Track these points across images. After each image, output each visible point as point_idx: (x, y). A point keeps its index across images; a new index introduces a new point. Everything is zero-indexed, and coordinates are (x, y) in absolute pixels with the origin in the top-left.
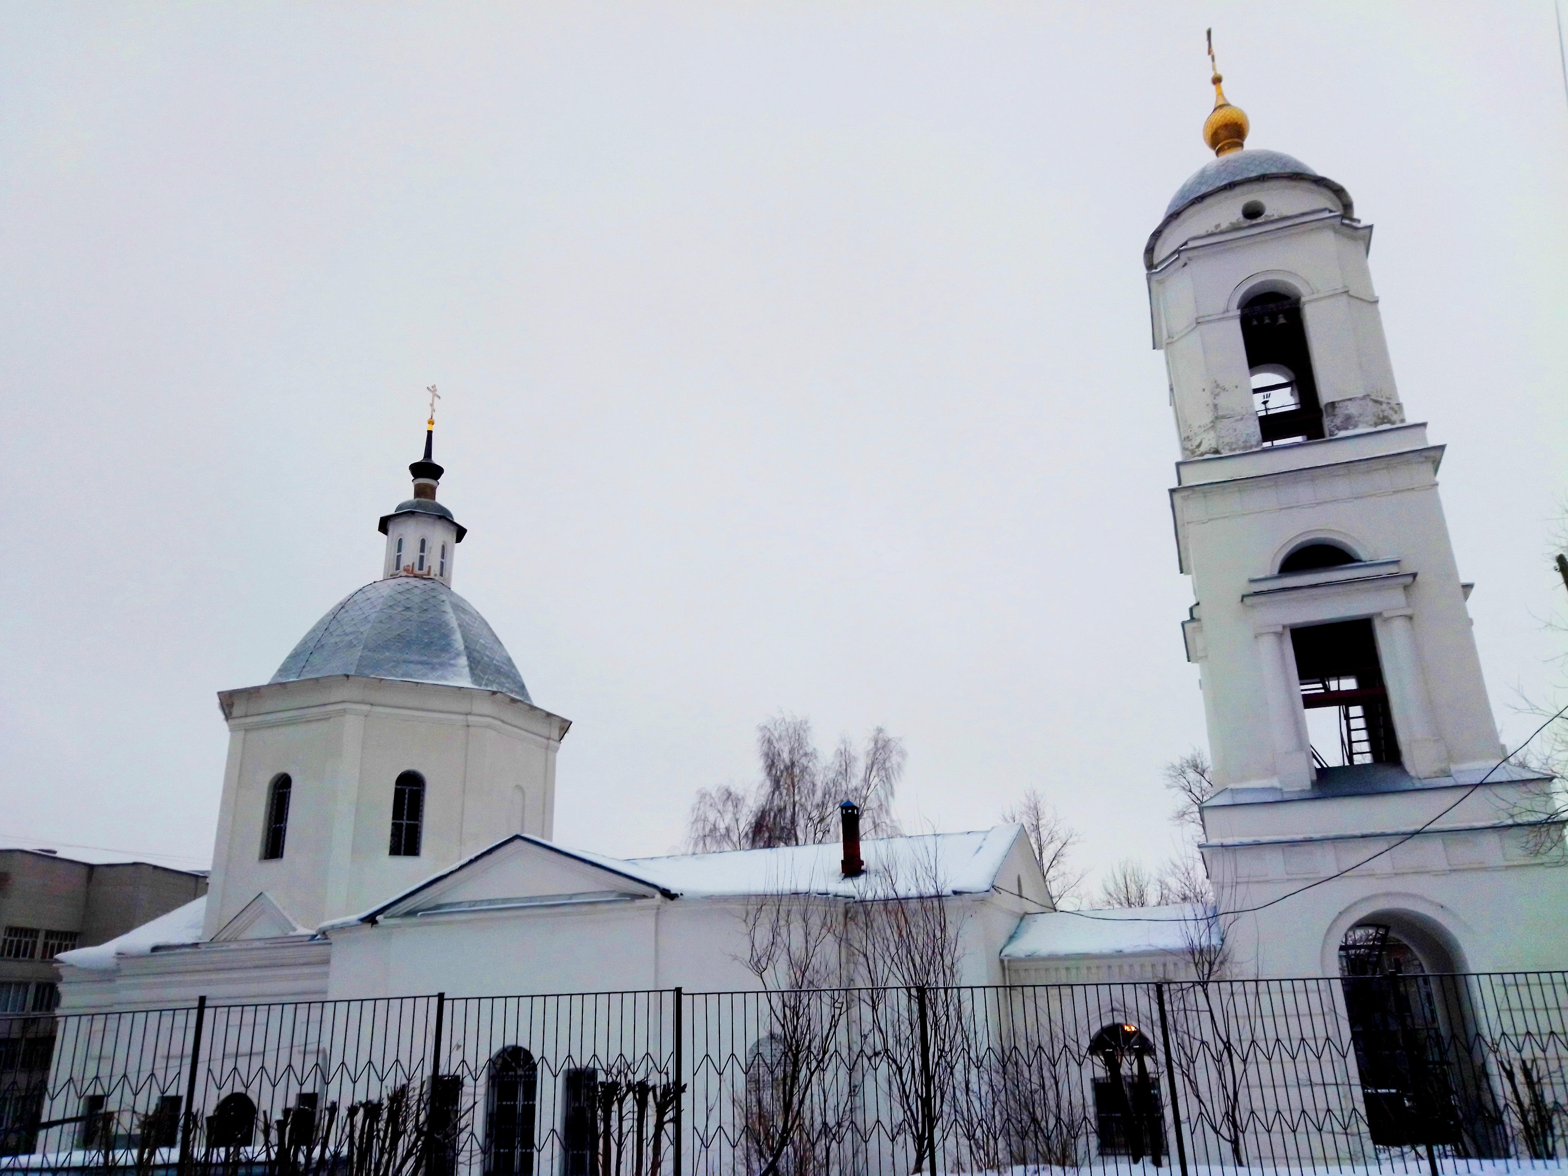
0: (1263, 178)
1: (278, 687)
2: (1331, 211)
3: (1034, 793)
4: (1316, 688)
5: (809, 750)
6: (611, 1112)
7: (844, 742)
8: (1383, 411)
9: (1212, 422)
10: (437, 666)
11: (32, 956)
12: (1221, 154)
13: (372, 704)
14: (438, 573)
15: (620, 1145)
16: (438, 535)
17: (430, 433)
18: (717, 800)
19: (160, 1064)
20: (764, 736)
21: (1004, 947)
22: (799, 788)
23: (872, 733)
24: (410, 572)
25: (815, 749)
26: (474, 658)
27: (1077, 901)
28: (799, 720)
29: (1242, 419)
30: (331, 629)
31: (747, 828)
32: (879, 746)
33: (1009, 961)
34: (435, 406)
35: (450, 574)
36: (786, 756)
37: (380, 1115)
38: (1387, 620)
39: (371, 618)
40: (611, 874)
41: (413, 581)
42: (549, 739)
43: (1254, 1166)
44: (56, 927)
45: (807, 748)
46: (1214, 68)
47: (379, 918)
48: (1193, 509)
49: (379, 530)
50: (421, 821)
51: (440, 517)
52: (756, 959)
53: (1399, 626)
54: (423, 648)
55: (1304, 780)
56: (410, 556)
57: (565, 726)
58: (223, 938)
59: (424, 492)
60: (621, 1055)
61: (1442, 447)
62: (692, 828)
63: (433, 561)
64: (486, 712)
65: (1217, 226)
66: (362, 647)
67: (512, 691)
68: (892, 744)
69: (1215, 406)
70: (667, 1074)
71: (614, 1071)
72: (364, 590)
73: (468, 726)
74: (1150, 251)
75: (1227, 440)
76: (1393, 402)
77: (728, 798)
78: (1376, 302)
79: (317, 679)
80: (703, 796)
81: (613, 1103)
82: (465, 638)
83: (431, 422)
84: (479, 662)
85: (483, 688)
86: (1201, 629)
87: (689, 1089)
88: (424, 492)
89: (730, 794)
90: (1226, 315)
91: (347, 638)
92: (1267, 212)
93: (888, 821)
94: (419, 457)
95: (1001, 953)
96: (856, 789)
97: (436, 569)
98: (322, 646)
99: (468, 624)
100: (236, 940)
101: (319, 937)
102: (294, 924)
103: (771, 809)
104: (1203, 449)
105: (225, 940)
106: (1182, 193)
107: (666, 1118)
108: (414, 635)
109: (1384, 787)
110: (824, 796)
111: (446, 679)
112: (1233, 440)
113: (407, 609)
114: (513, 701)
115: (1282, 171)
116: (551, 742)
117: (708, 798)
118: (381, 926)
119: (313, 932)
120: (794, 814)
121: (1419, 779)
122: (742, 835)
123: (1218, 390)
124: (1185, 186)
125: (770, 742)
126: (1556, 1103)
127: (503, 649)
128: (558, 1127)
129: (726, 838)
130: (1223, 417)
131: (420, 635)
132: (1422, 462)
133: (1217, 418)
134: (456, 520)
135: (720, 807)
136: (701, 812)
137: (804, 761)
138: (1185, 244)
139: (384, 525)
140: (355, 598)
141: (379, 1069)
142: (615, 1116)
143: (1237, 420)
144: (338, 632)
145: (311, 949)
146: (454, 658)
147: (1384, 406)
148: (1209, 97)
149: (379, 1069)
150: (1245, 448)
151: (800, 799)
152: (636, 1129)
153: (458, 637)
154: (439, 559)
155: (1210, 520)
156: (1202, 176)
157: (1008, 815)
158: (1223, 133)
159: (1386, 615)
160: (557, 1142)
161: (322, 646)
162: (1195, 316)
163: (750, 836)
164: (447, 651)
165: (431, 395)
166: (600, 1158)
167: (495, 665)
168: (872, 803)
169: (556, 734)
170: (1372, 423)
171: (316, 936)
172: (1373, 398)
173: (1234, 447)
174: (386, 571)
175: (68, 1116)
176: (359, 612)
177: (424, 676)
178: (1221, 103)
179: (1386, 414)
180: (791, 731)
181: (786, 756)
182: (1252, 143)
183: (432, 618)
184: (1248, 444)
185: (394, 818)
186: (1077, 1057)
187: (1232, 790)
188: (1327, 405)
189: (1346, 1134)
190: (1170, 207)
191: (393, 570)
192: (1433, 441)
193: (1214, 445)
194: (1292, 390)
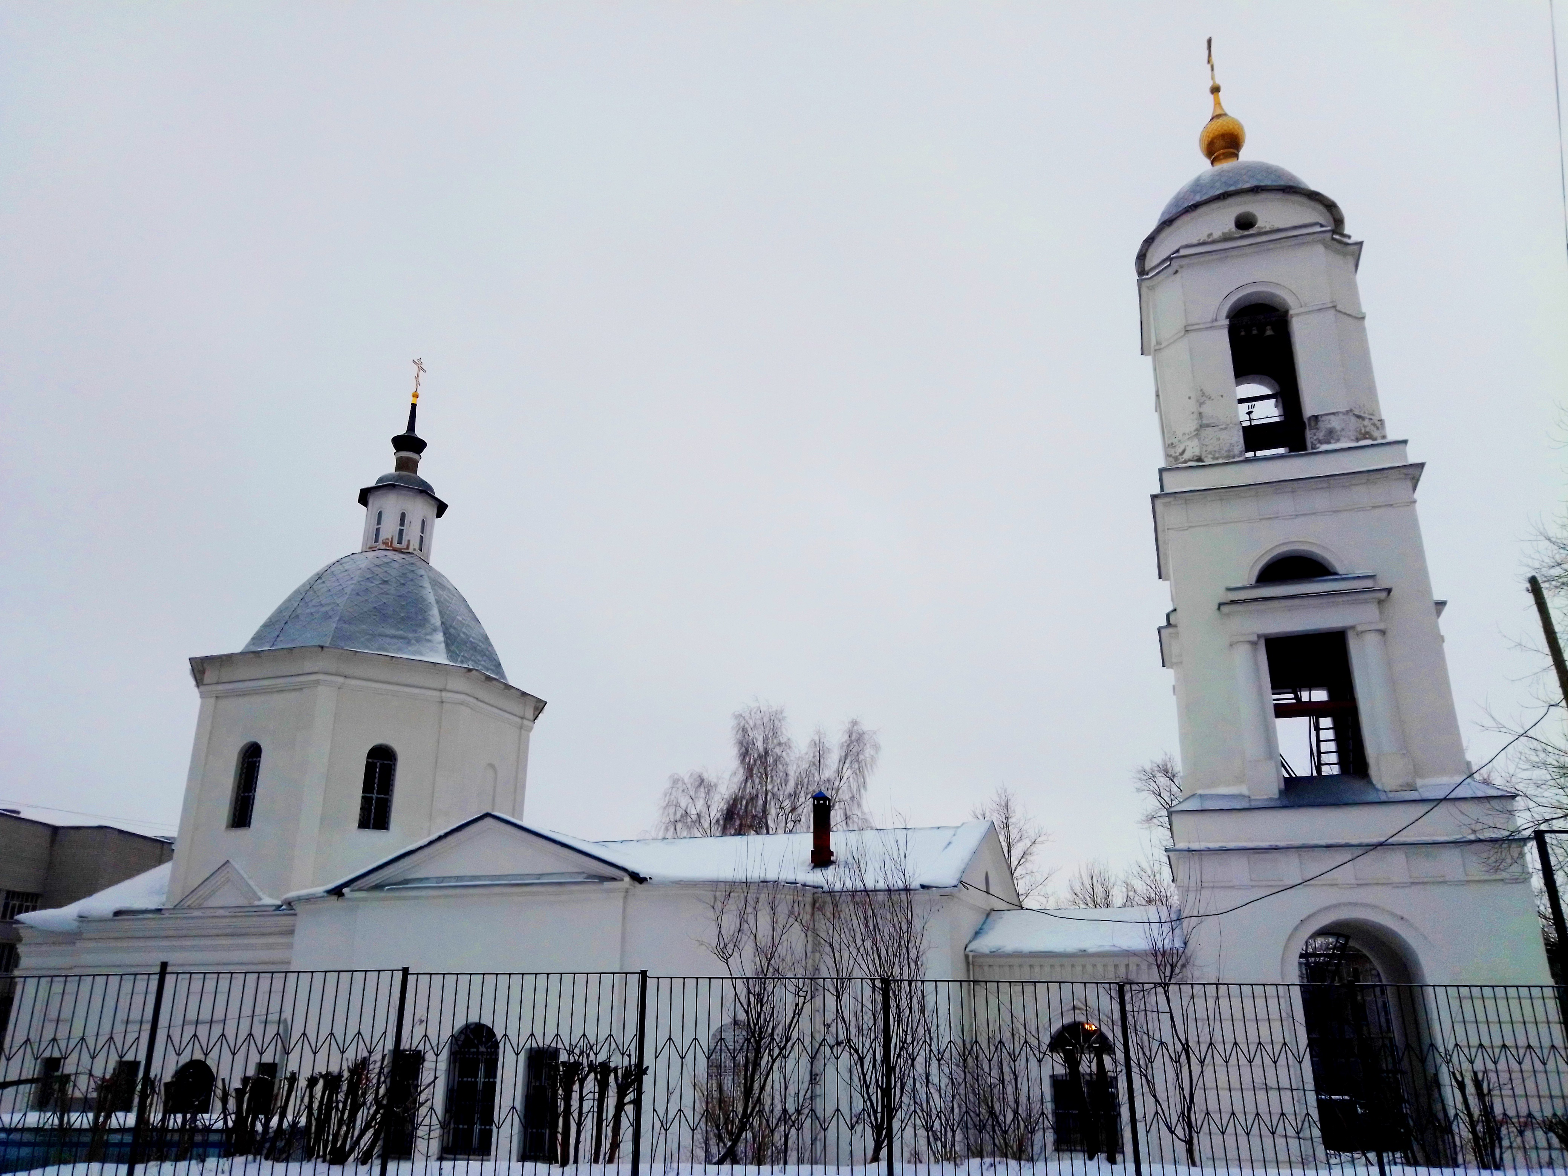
0: (1256, 190)
1: (251, 655)
2: (1322, 226)
3: (1005, 791)
4: (1287, 698)
5: (783, 740)
6: (572, 1091)
7: (819, 733)
8: (1365, 427)
9: (1197, 430)
15: (579, 1124)
16: (418, 509)
17: (414, 406)
18: (689, 786)
20: (739, 724)
21: (970, 942)
22: (772, 777)
23: (847, 726)
24: (389, 546)
26: (450, 634)
27: (1044, 900)
28: (774, 709)
29: (1226, 428)
31: (719, 815)
33: (974, 957)
34: (420, 379)
36: (760, 745)
41: (390, 554)
46: (1213, 78)
47: (346, 890)
48: (1174, 516)
49: (359, 501)
50: (391, 796)
51: (421, 492)
52: (722, 945)
56: (389, 529)
57: (539, 706)
59: (406, 466)
60: (584, 1035)
61: (1422, 465)
62: (663, 813)
63: (412, 534)
65: (1210, 235)
68: (866, 737)
69: (1200, 413)
70: (629, 1056)
71: (577, 1051)
72: (343, 561)
73: (442, 702)
74: (1141, 257)
75: (1210, 448)
76: (1375, 419)
78: (1363, 318)
79: (291, 649)
80: (676, 781)
81: (574, 1083)
83: (416, 396)
87: (650, 1071)
88: (406, 466)
89: (702, 781)
90: (1215, 324)
91: (323, 609)
92: (1260, 224)
94: (402, 430)
96: (829, 781)
97: (415, 544)
99: (445, 600)
100: (200, 908)
102: (260, 894)
103: (742, 798)
104: (1186, 456)
105: (189, 907)
106: (1177, 200)
107: (627, 1100)
110: (797, 785)
111: (421, 654)
112: (1216, 449)
113: (385, 582)
114: (488, 678)
116: (525, 722)
117: (680, 784)
118: (349, 899)
119: (279, 903)
120: (766, 802)
121: (1385, 792)
122: (714, 821)
124: (1179, 193)
125: (744, 730)
126: (1555, 1115)
128: (518, 1105)
129: (697, 825)
130: (1208, 426)
133: (1201, 426)
134: (437, 495)
135: (692, 793)
136: (672, 797)
137: (778, 750)
138: (1177, 251)
139: (365, 497)
140: (332, 569)
142: (575, 1096)
143: (1222, 429)
146: (430, 634)
147: (1366, 422)
150: (1228, 457)
151: (773, 789)
153: (435, 611)
155: (1190, 527)
156: (1197, 185)
157: (979, 812)
158: (1219, 143)
159: (1360, 628)
160: (516, 1119)
166: (560, 1137)
169: (530, 714)
170: (1354, 438)
172: (1357, 413)
173: (1217, 455)
174: (365, 543)
175: (23, 1077)
177: (399, 650)
178: (1219, 112)
179: (1367, 429)
180: (766, 720)
181: (760, 745)
182: (1247, 154)
185: (363, 792)
186: (1037, 1053)
187: (1201, 795)
188: (1309, 419)
190: (1163, 214)
191: (371, 543)
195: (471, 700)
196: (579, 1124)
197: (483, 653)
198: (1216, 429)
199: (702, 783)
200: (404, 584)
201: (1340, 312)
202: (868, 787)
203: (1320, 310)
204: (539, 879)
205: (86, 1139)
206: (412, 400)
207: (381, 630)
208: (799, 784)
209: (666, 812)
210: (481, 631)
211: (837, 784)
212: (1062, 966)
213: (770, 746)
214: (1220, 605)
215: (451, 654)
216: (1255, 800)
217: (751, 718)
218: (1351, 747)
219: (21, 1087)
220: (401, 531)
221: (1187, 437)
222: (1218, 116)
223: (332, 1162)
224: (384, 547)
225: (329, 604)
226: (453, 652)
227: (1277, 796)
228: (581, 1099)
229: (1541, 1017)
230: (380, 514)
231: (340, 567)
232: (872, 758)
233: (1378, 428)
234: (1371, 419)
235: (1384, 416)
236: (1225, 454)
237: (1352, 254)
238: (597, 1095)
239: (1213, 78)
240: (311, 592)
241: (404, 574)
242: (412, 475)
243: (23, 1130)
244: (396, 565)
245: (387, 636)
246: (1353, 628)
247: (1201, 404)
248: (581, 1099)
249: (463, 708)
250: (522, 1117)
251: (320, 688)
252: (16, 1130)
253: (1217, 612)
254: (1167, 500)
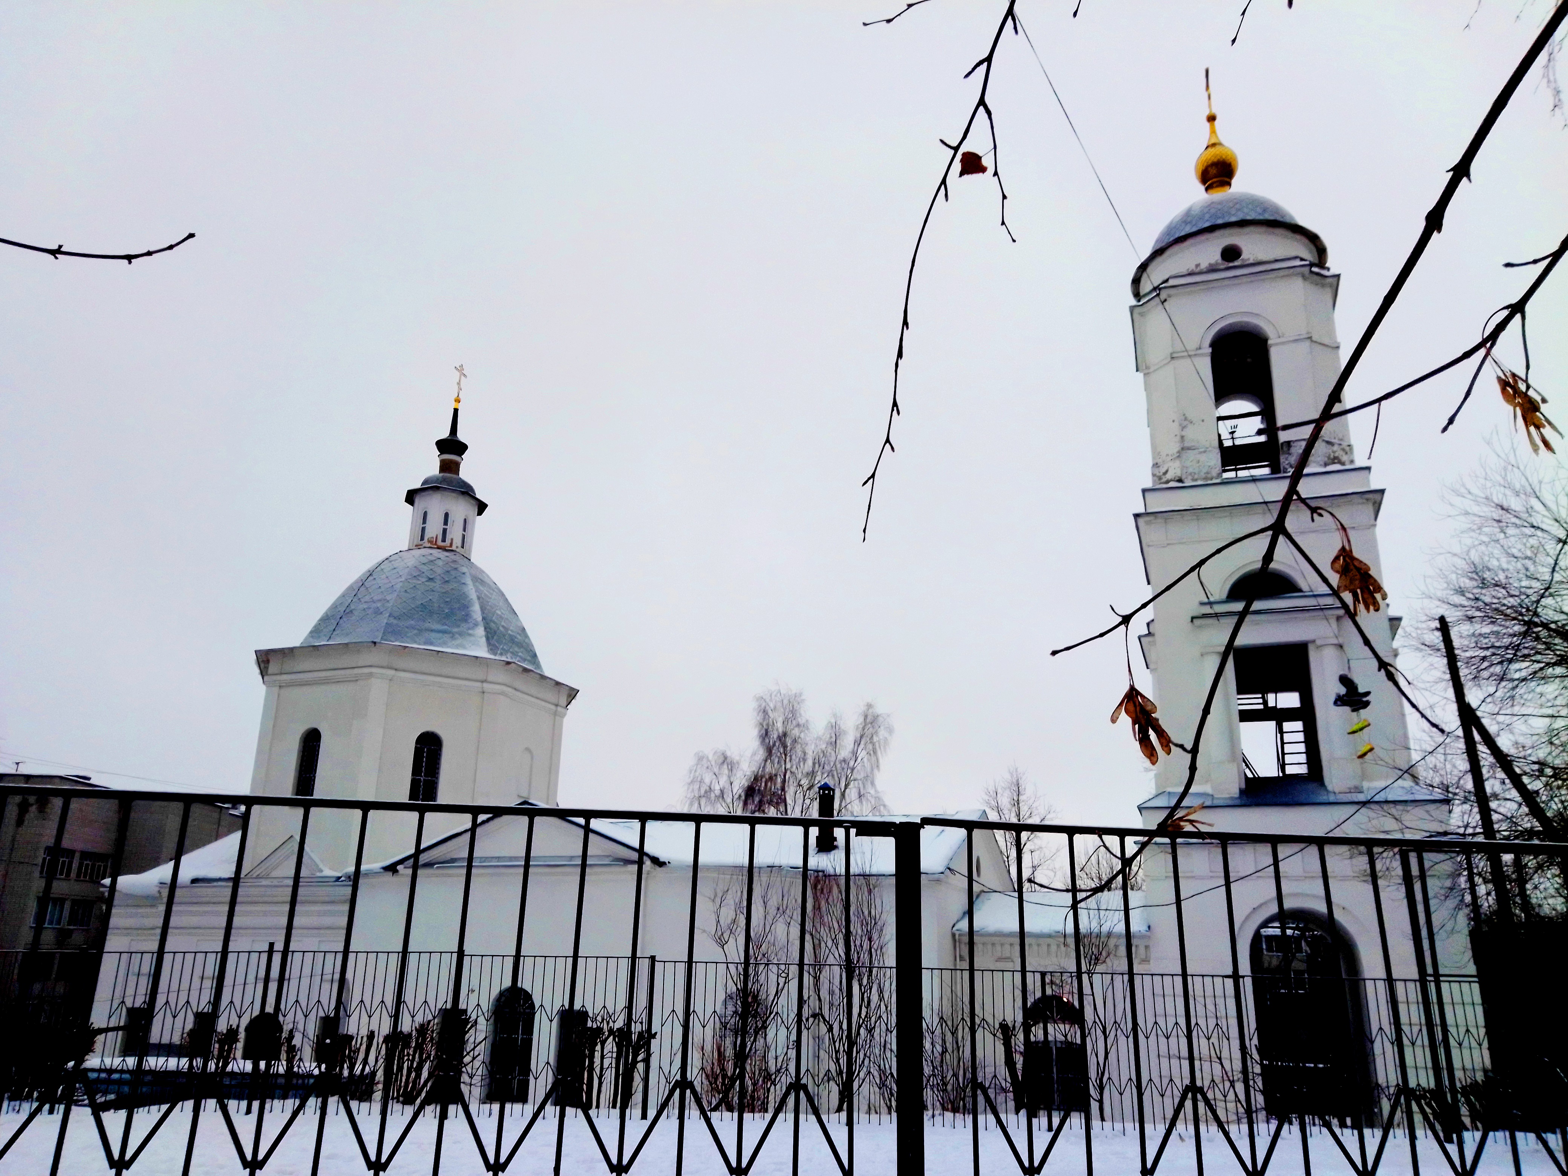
0: (1243, 224)
1: (309, 650)
2: (1302, 259)
3: (1016, 770)
4: (1253, 702)
5: (802, 721)
6: (595, 1051)
7: (835, 715)
8: (1334, 452)
9: (1178, 452)
10: (457, 636)
11: (68, 874)
12: (1210, 191)
13: (396, 670)
14: (460, 545)
15: (600, 1078)
16: (460, 509)
17: (456, 411)
18: (713, 763)
20: (760, 706)
21: (958, 921)
22: (791, 756)
23: (863, 708)
24: (434, 545)
25: (807, 721)
26: (490, 629)
27: (1051, 874)
28: (794, 692)
29: (1205, 452)
30: (359, 596)
31: (740, 791)
32: (868, 721)
33: (960, 935)
35: (470, 547)
36: (779, 726)
37: (410, 1043)
38: (1319, 647)
39: (398, 586)
40: (607, 841)
41: (436, 552)
42: (557, 705)
43: (1128, 1122)
44: (89, 848)
45: (799, 720)
46: (1210, 105)
47: (399, 867)
48: (1154, 533)
49: (406, 501)
50: (437, 778)
51: (463, 493)
52: (719, 933)
53: (1330, 653)
54: (444, 618)
55: (1232, 788)
56: (434, 529)
57: (572, 693)
58: (254, 876)
59: (449, 468)
60: (604, 1007)
61: (1382, 492)
62: (688, 789)
63: (455, 534)
64: (500, 681)
65: (1197, 266)
66: (388, 615)
67: (525, 660)
68: (880, 719)
69: (1182, 437)
70: (641, 1023)
71: (599, 1018)
72: (391, 559)
73: (483, 692)
74: (1136, 282)
75: (1190, 470)
76: (1345, 444)
77: (724, 762)
78: (1338, 347)
79: (347, 644)
80: (700, 758)
81: (597, 1044)
82: (483, 609)
83: (458, 401)
84: (495, 633)
85: (497, 658)
86: (1154, 643)
87: (658, 1036)
88: (449, 468)
89: (726, 758)
90: (1199, 352)
91: (374, 605)
92: (1244, 256)
93: (872, 792)
94: (445, 434)
95: (953, 926)
96: (844, 761)
97: (457, 542)
98: (351, 612)
99: (485, 595)
100: (267, 877)
101: (343, 879)
102: (321, 866)
103: (762, 777)
104: (1169, 476)
105: (258, 877)
106: (1170, 229)
107: (640, 1058)
108: (436, 605)
109: (1302, 798)
110: (814, 764)
111: (464, 648)
112: (1196, 471)
113: (430, 579)
114: (526, 670)
115: (1261, 217)
116: (559, 709)
117: (705, 760)
118: (402, 875)
119: (340, 875)
120: (784, 781)
121: (1335, 793)
122: (736, 797)
123: (1185, 423)
124: (1171, 223)
125: (765, 712)
126: (1419, 1085)
127: (518, 620)
128: (552, 1061)
129: (721, 799)
130: (1189, 449)
131: (442, 606)
132: (1363, 503)
133: (1183, 449)
134: (478, 496)
135: (716, 770)
136: (697, 774)
137: (796, 732)
138: (1166, 281)
139: (411, 497)
140: (382, 566)
142: (598, 1055)
143: (1201, 453)
144: (367, 598)
145: (337, 889)
146: (472, 628)
147: (1336, 448)
148: (1202, 135)
150: (1206, 479)
151: (792, 767)
152: (614, 1065)
153: (476, 608)
154: (461, 532)
155: (1168, 544)
156: (1188, 216)
157: (991, 789)
158: (1213, 171)
159: (1318, 642)
160: (550, 1073)
161: (351, 612)
162: (1171, 350)
163: (743, 798)
164: (466, 621)
165: (458, 374)
166: (585, 1087)
167: (510, 635)
168: (858, 774)
169: (563, 702)
170: (1322, 463)
171: (340, 877)
172: (1326, 439)
173: (1196, 477)
174: (411, 540)
175: (111, 1025)
176: (386, 581)
177: (444, 644)
178: (1213, 141)
179: (1336, 455)
180: (786, 702)
181: (779, 726)
182: (1240, 185)
183: (452, 589)
184: (1209, 476)
185: (413, 774)
186: (986, 1026)
187: (1169, 793)
188: (1282, 444)
189: (1225, 1101)
190: (1157, 241)
191: (417, 541)
192: (1375, 484)
193: (1179, 474)
194: (1262, 418)
195: (510, 690)
196: (600, 1078)
197: (520, 645)
198: (1196, 451)
199: (725, 760)
200: (447, 582)
201: (1316, 342)
202: (882, 767)
203: (1296, 341)
204: (570, 861)
205: (281, 1081)
206: (453, 405)
207: (427, 625)
208: (816, 762)
209: (691, 787)
211: (852, 763)
212: (1039, 945)
213: (788, 729)
214: (1193, 619)
215: (492, 648)
216: (1218, 798)
217: (771, 700)
219: (110, 1034)
220: (445, 531)
221: (1169, 458)
222: (1214, 145)
223: (404, 1103)
224: (429, 545)
225: (380, 600)
226: (494, 645)
227: (1237, 795)
228: (602, 1057)
229: (1467, 999)
230: (425, 514)
231: (390, 564)
232: (886, 739)
233: (1346, 453)
234: (1340, 445)
235: (1353, 442)
236: (1204, 476)
237: (1331, 286)
238: (615, 1055)
239: (1210, 105)
240: (362, 589)
241: (448, 572)
242: (454, 476)
243: (122, 1071)
244: (440, 563)
245: (432, 631)
246: (1314, 641)
247: (1183, 428)
248: (602, 1057)
249: (501, 697)
250: (555, 1070)
251: (373, 680)
252: (116, 1071)
253: (1190, 624)
254: (1147, 518)
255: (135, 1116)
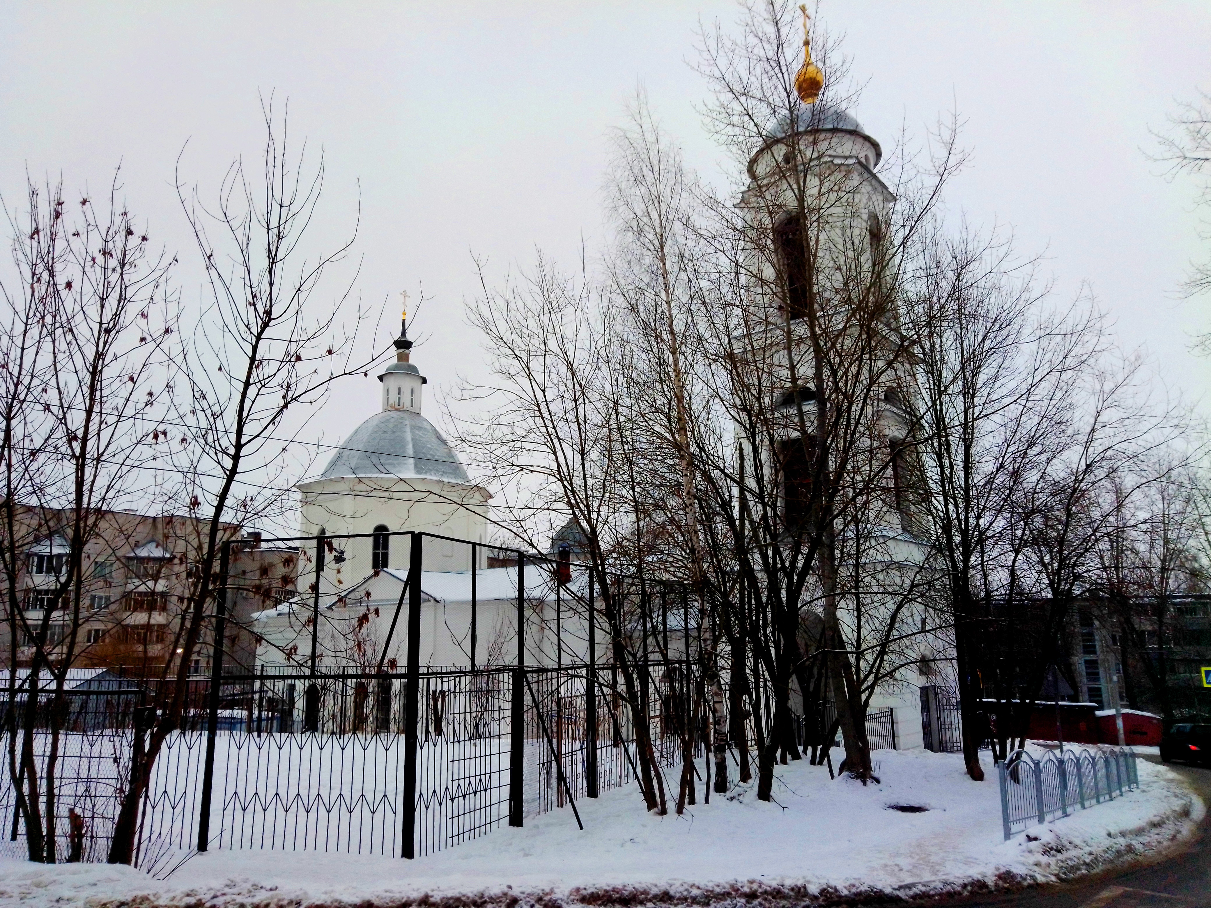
16: (407, 384)
17: (404, 321)
19: (450, 783)
34: (407, 303)
56: (393, 398)
59: (403, 358)
63: (406, 400)
82: (414, 446)
83: (404, 314)
88: (403, 358)
97: (408, 404)
104: (645, 345)
113: (385, 432)
141: (326, 801)
149: (326, 801)
154: (409, 397)
210: (77, 663)
215: (418, 470)
218: (1060, 703)
220: (399, 398)
244: (393, 420)
255: (217, 739)
